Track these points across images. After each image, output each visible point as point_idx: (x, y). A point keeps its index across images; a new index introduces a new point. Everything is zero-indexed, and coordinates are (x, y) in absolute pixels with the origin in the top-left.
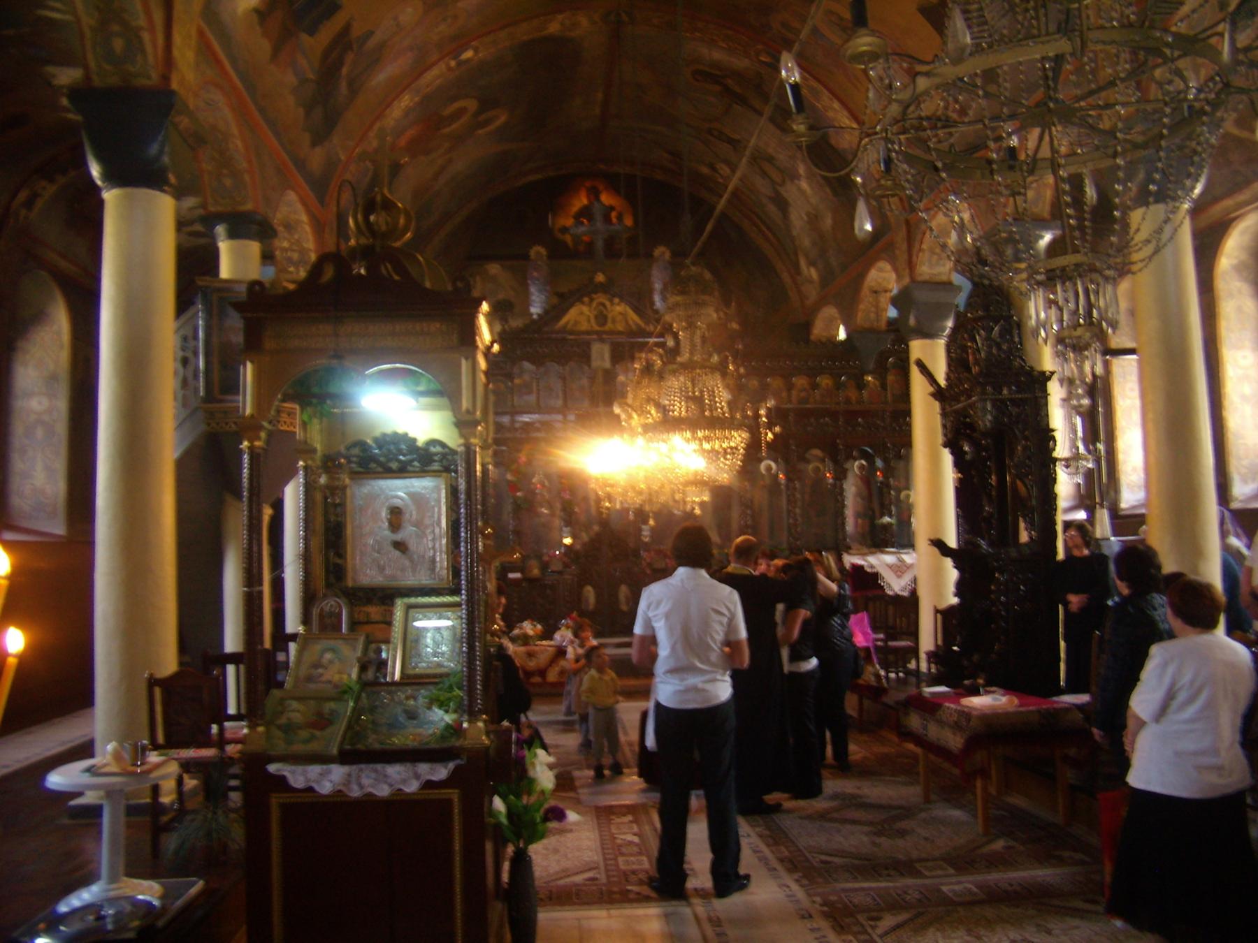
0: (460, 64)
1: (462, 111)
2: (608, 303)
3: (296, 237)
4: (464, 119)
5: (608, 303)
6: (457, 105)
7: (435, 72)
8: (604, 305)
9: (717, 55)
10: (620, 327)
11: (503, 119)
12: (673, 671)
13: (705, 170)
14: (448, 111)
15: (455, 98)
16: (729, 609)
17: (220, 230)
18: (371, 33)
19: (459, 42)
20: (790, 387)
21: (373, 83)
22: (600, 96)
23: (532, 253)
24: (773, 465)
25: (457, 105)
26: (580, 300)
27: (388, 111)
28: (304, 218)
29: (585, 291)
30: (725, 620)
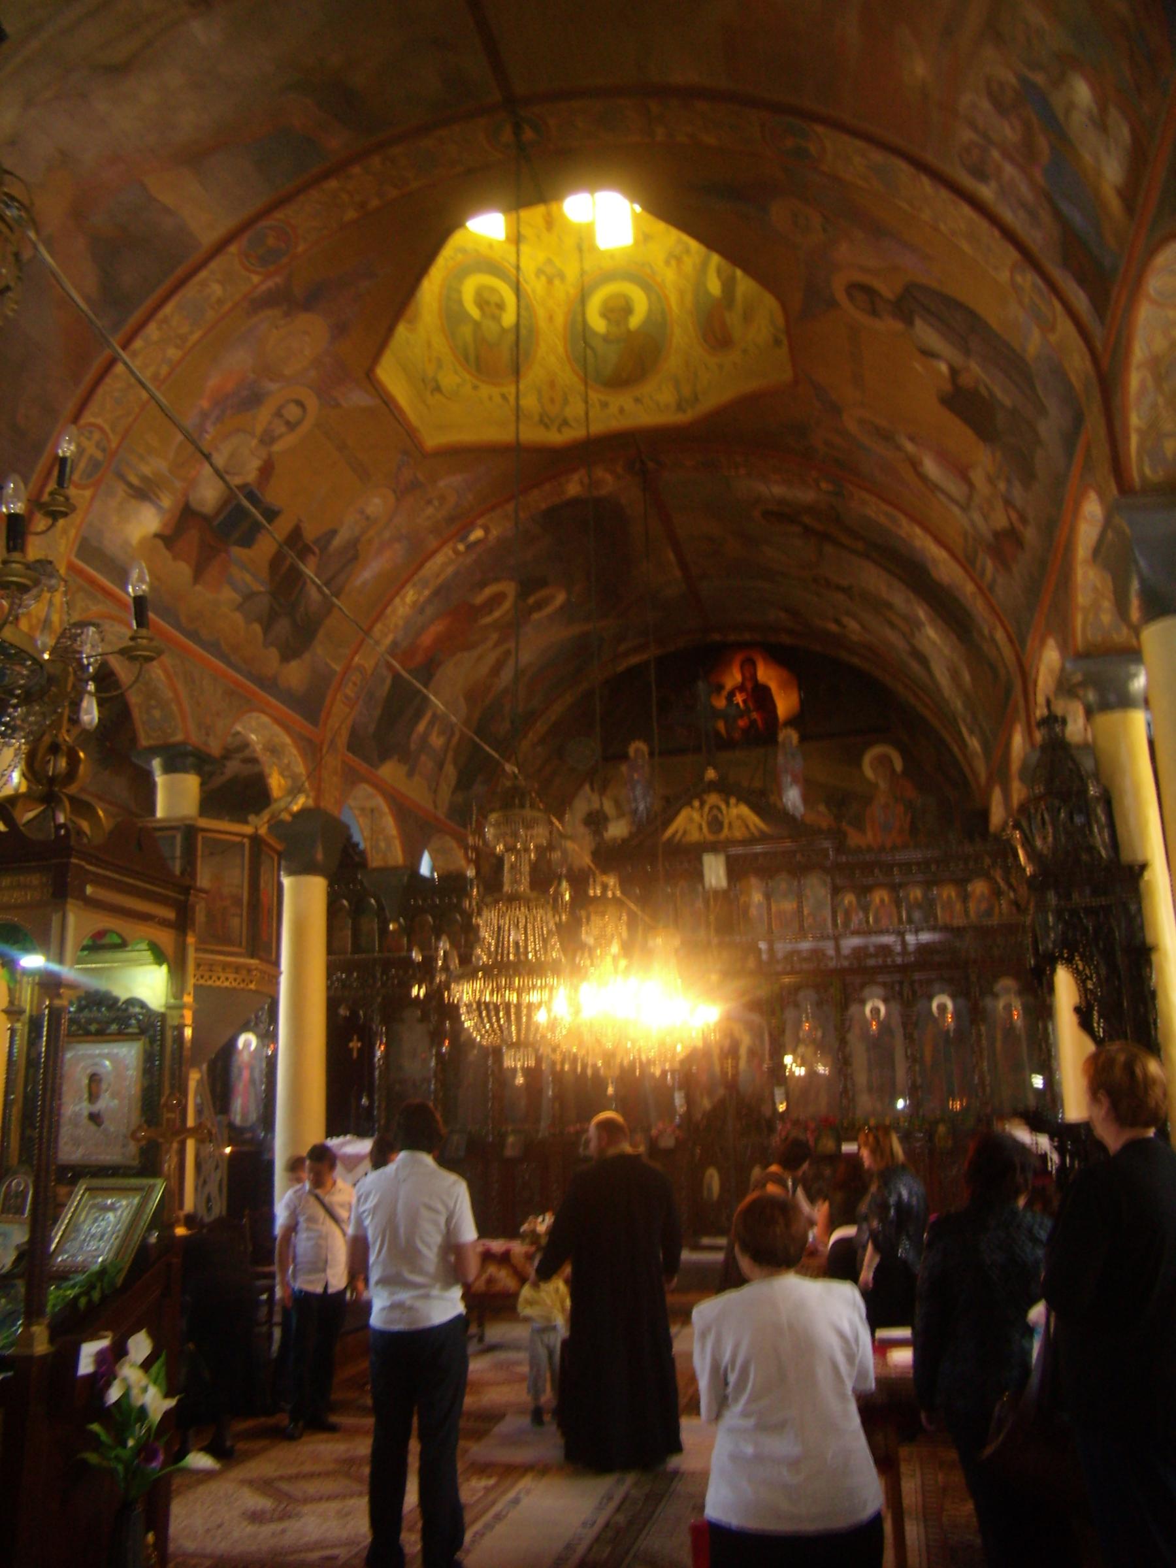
0: (470, 547)
1: (498, 598)
2: (723, 807)
3: (286, 761)
4: (507, 605)
5: (723, 807)
6: (489, 591)
7: (439, 559)
8: (719, 809)
9: (778, 490)
10: (738, 834)
11: (560, 598)
12: (384, 1281)
13: (833, 627)
14: (480, 599)
15: (483, 585)
16: (446, 1206)
17: (156, 764)
18: (333, 533)
19: (459, 524)
20: (965, 898)
21: (358, 582)
22: (671, 556)
23: (631, 751)
24: (950, 1005)
25: (489, 591)
26: (689, 803)
27: (389, 610)
28: (288, 740)
29: (692, 792)
30: (442, 1220)
